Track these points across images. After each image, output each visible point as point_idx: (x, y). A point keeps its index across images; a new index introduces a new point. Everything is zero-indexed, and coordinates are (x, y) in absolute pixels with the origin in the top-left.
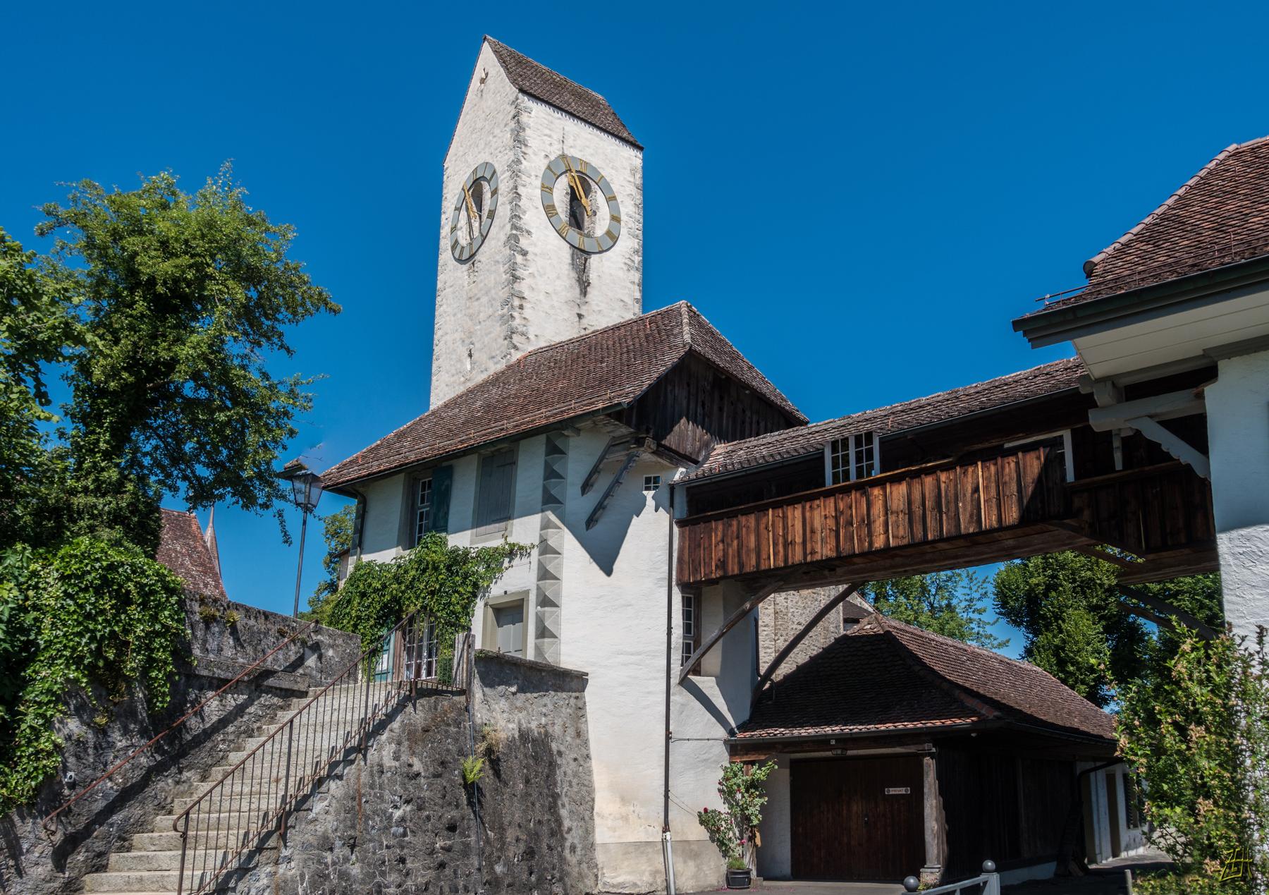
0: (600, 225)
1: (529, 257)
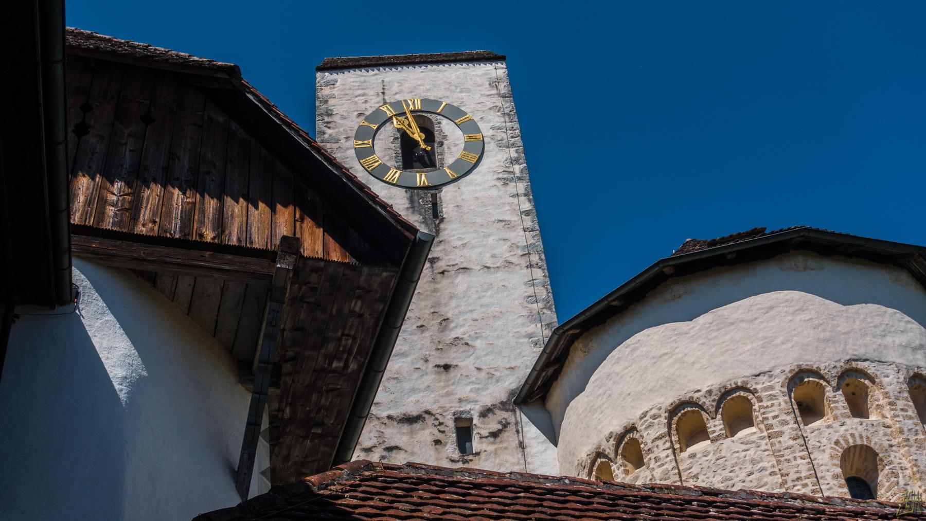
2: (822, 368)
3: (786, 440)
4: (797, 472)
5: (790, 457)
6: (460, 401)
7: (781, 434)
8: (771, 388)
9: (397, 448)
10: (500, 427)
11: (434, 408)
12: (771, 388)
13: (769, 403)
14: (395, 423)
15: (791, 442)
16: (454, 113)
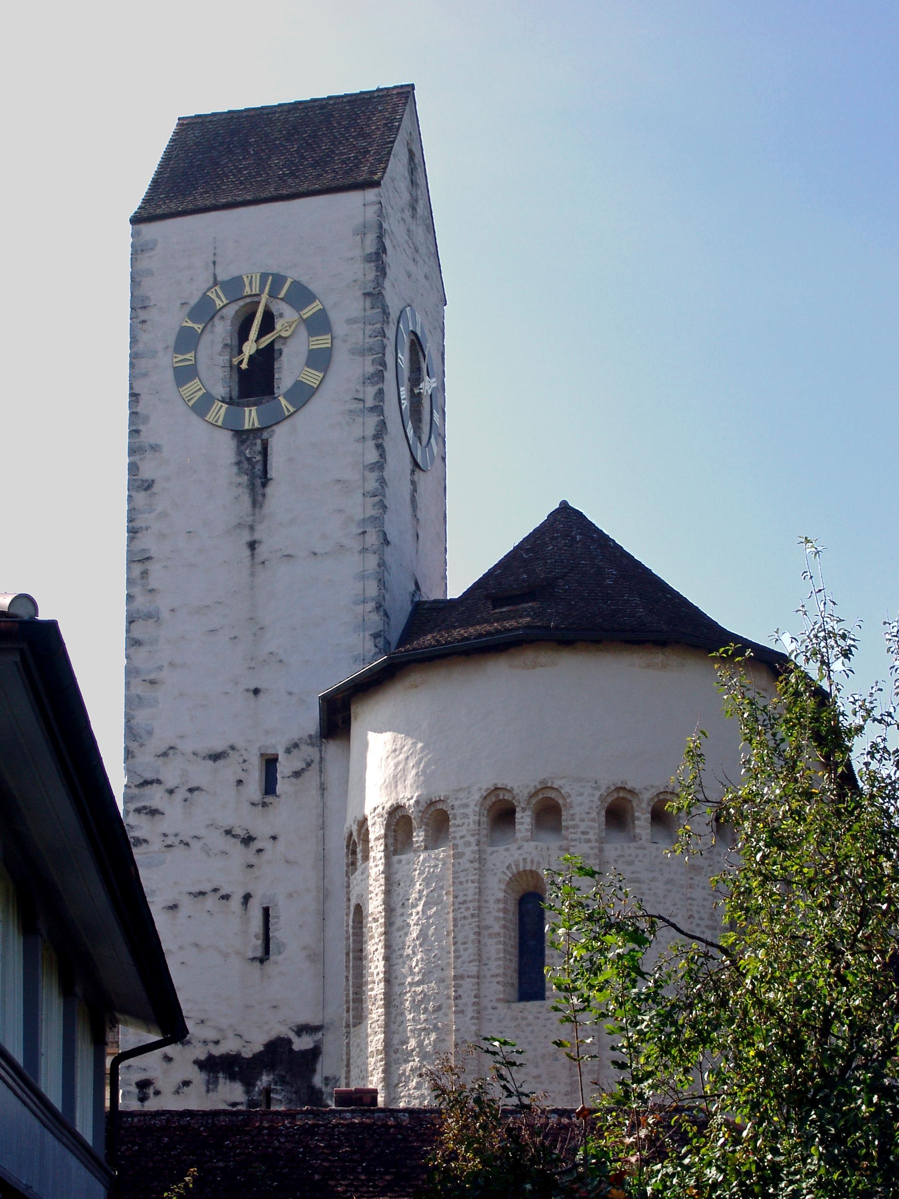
0: (290, 371)
1: (156, 488)
2: (515, 788)
4: (465, 895)
5: (464, 879)
6: (267, 732)
8: (466, 806)
9: (197, 789)
10: (304, 766)
11: (240, 743)
12: (466, 806)
13: (461, 822)
14: (199, 760)
15: (468, 865)
16: (301, 295)
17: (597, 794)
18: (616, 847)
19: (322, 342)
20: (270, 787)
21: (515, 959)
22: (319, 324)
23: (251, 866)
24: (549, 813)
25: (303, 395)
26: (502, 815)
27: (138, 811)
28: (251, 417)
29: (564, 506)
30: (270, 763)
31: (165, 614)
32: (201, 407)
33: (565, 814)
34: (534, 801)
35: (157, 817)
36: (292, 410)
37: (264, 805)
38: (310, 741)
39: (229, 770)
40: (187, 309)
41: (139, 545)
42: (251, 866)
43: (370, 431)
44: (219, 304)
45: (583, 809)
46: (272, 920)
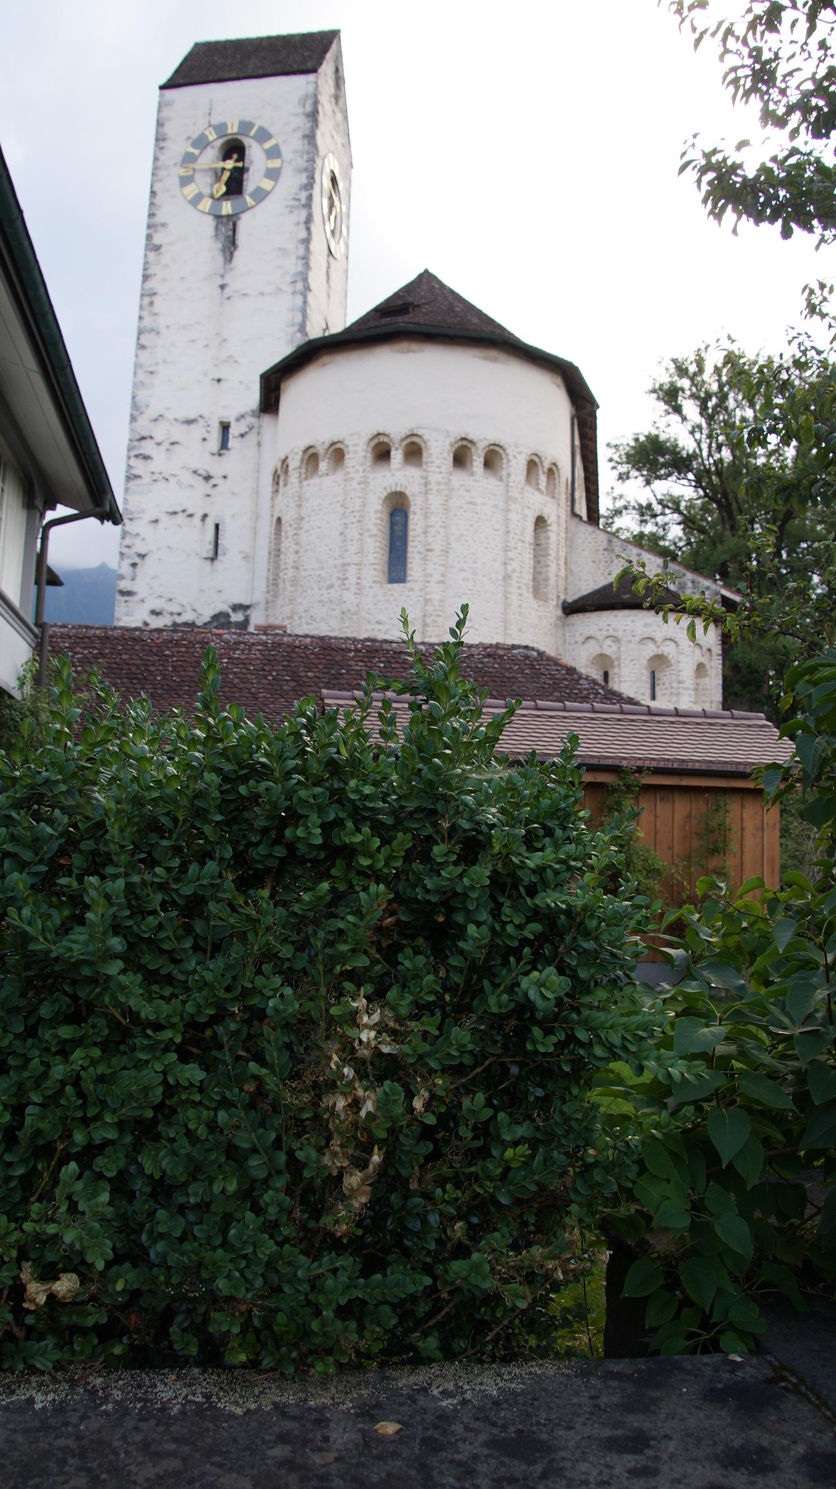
0: (253, 181)
3: (354, 484)
6: (224, 407)
7: (352, 479)
8: (357, 445)
9: (177, 443)
11: (206, 414)
12: (357, 445)
16: (263, 135)
17: (448, 441)
18: (459, 478)
19: (275, 164)
20: (224, 445)
21: (387, 555)
22: (274, 153)
23: (209, 495)
24: (414, 452)
25: (261, 195)
26: (382, 453)
27: (137, 456)
28: (227, 208)
29: (426, 271)
30: (225, 427)
31: (162, 330)
32: (195, 201)
33: (425, 454)
34: (404, 443)
35: (149, 461)
36: (253, 203)
37: (220, 455)
38: (253, 414)
39: (197, 431)
40: (190, 141)
41: (148, 285)
42: (209, 495)
43: (303, 219)
44: (211, 138)
45: (438, 452)
46: (220, 532)
